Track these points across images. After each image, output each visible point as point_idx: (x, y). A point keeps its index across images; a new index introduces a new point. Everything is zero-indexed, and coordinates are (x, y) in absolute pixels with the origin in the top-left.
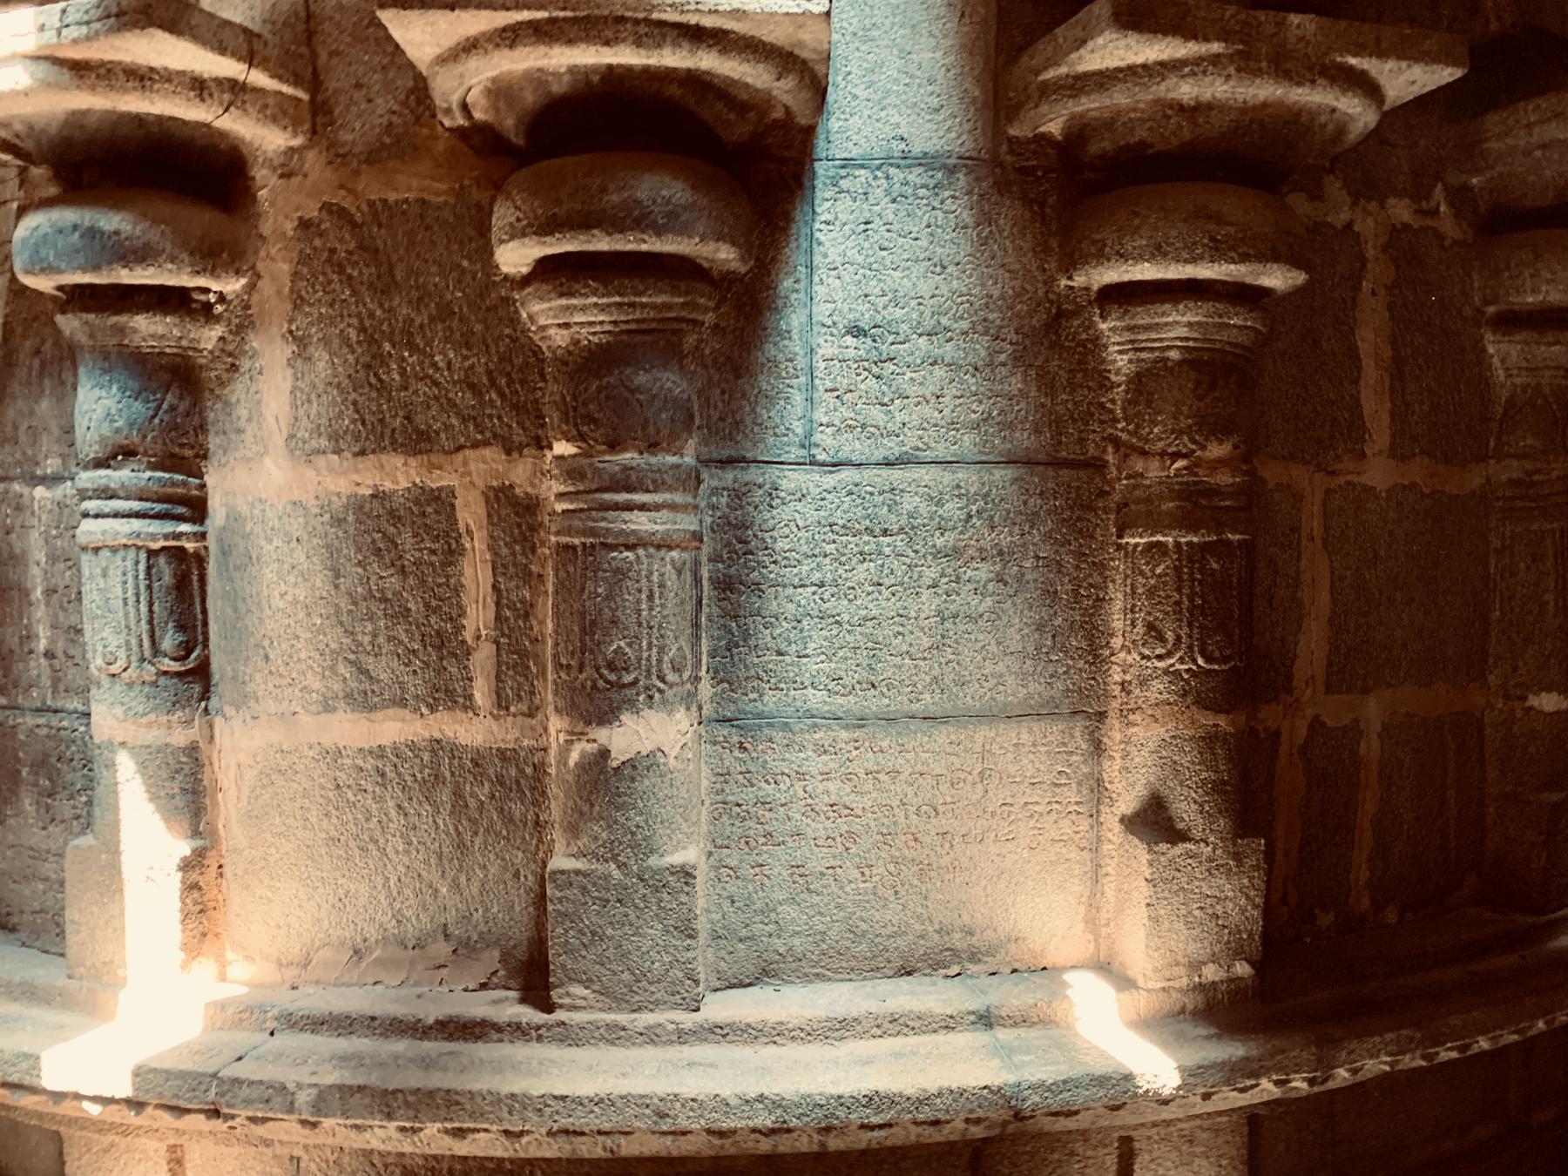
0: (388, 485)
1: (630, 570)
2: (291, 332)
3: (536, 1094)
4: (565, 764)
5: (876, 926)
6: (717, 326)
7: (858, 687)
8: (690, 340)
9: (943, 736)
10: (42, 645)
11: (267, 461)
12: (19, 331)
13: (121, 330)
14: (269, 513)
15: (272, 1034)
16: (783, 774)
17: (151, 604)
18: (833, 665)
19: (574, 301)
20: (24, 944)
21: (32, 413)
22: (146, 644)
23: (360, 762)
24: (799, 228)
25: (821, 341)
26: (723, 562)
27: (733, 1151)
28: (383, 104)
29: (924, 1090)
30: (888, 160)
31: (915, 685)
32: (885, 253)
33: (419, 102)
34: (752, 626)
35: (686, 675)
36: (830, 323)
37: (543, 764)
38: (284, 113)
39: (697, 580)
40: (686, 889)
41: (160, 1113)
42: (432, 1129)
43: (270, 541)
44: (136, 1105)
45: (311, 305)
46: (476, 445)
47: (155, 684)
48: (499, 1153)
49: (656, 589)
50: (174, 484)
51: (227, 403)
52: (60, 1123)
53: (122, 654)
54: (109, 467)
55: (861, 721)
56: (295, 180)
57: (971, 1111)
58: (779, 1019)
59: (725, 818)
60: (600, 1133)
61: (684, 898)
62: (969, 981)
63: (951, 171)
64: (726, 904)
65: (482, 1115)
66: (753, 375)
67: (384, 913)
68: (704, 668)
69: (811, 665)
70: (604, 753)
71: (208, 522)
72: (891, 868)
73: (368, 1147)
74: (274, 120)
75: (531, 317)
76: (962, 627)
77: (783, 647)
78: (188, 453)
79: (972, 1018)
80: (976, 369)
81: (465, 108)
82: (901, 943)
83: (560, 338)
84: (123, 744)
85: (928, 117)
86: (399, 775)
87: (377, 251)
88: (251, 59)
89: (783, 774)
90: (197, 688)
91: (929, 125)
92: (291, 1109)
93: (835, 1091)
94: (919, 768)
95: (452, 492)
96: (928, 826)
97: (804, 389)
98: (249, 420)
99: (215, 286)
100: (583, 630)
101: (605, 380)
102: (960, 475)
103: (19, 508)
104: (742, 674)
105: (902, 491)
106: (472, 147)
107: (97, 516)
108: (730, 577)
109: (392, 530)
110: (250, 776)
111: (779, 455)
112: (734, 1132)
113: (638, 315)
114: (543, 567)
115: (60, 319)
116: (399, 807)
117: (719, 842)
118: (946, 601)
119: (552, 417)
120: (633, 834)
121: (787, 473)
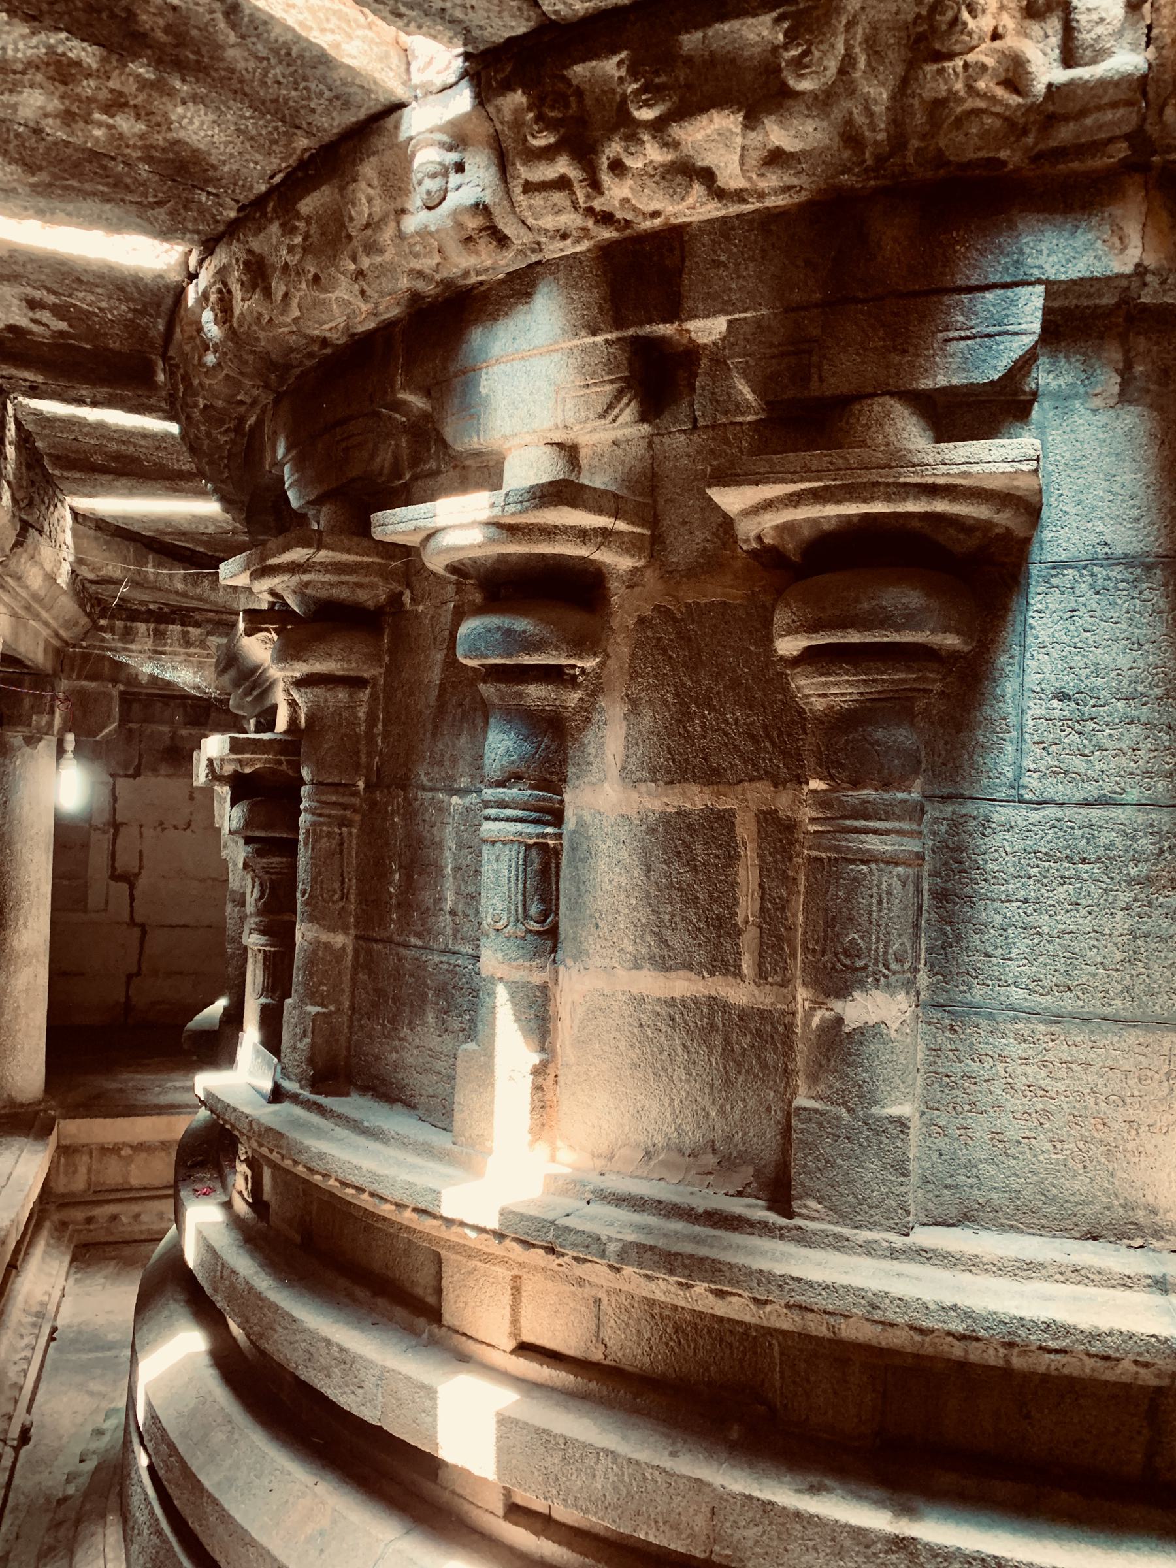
0: (688, 806)
1: (864, 880)
2: (627, 696)
3: (778, 1273)
4: (809, 1026)
5: (1066, 1193)
6: (943, 692)
7: (1055, 988)
8: (920, 704)
9: (1132, 1037)
10: (449, 905)
11: (606, 785)
12: (450, 690)
13: (520, 695)
14: (605, 823)
15: (588, 1203)
16: (987, 1055)
17: (525, 883)
18: (1034, 969)
19: (831, 679)
20: (420, 1119)
21: (454, 746)
22: (520, 910)
23: (657, 1008)
24: (1014, 616)
25: (1031, 704)
26: (941, 878)
27: (930, 1351)
28: (700, 536)
29: (1097, 1328)
30: (1093, 561)
31: (1107, 992)
32: (1088, 634)
33: (725, 533)
34: (964, 931)
35: (907, 965)
36: (1039, 689)
37: (792, 1024)
38: (634, 545)
39: (919, 891)
40: (901, 1136)
41: (514, 1245)
42: (700, 1288)
43: (604, 842)
44: (500, 1236)
45: (642, 677)
46: (752, 780)
47: (523, 938)
48: (748, 1318)
49: (884, 895)
50: (544, 799)
51: (583, 744)
52: (443, 1247)
53: (505, 916)
54: (505, 786)
55: (1057, 1018)
56: (637, 590)
57: (1139, 1354)
58: (975, 1253)
59: (936, 1085)
60: (825, 1312)
61: (899, 1144)
62: (1151, 1254)
63: (1148, 568)
64: (935, 1155)
65: (738, 1282)
66: (973, 730)
67: (669, 1126)
68: (922, 961)
69: (1014, 968)
70: (839, 1020)
71: (564, 826)
72: (1081, 1145)
73: (650, 1296)
74: (627, 551)
75: (797, 687)
76: (1154, 946)
77: (990, 950)
78: (555, 778)
79: (1149, 1281)
80: (1170, 728)
81: (759, 538)
82: (1088, 1211)
83: (819, 704)
84: (501, 979)
85: (1129, 526)
86: (685, 1021)
87: (690, 639)
88: (616, 516)
89: (987, 1055)
90: (549, 944)
91: (1130, 532)
92: (603, 1254)
93: (1018, 1314)
94: (1109, 1063)
95: (733, 811)
96: (1116, 1114)
97: (1015, 741)
98: (596, 756)
99: (580, 664)
100: (826, 923)
101: (851, 736)
102: (1153, 816)
103: (441, 810)
104: (954, 970)
105: (1100, 827)
106: (762, 564)
107: (495, 820)
108: (947, 890)
109: (689, 839)
110: (580, 1011)
111: (992, 794)
112: (932, 1331)
113: (880, 688)
114: (797, 872)
115: (482, 687)
116: (684, 1045)
117: (931, 1104)
118: (1138, 922)
119: (809, 761)
120: (860, 1086)
121: (998, 808)
